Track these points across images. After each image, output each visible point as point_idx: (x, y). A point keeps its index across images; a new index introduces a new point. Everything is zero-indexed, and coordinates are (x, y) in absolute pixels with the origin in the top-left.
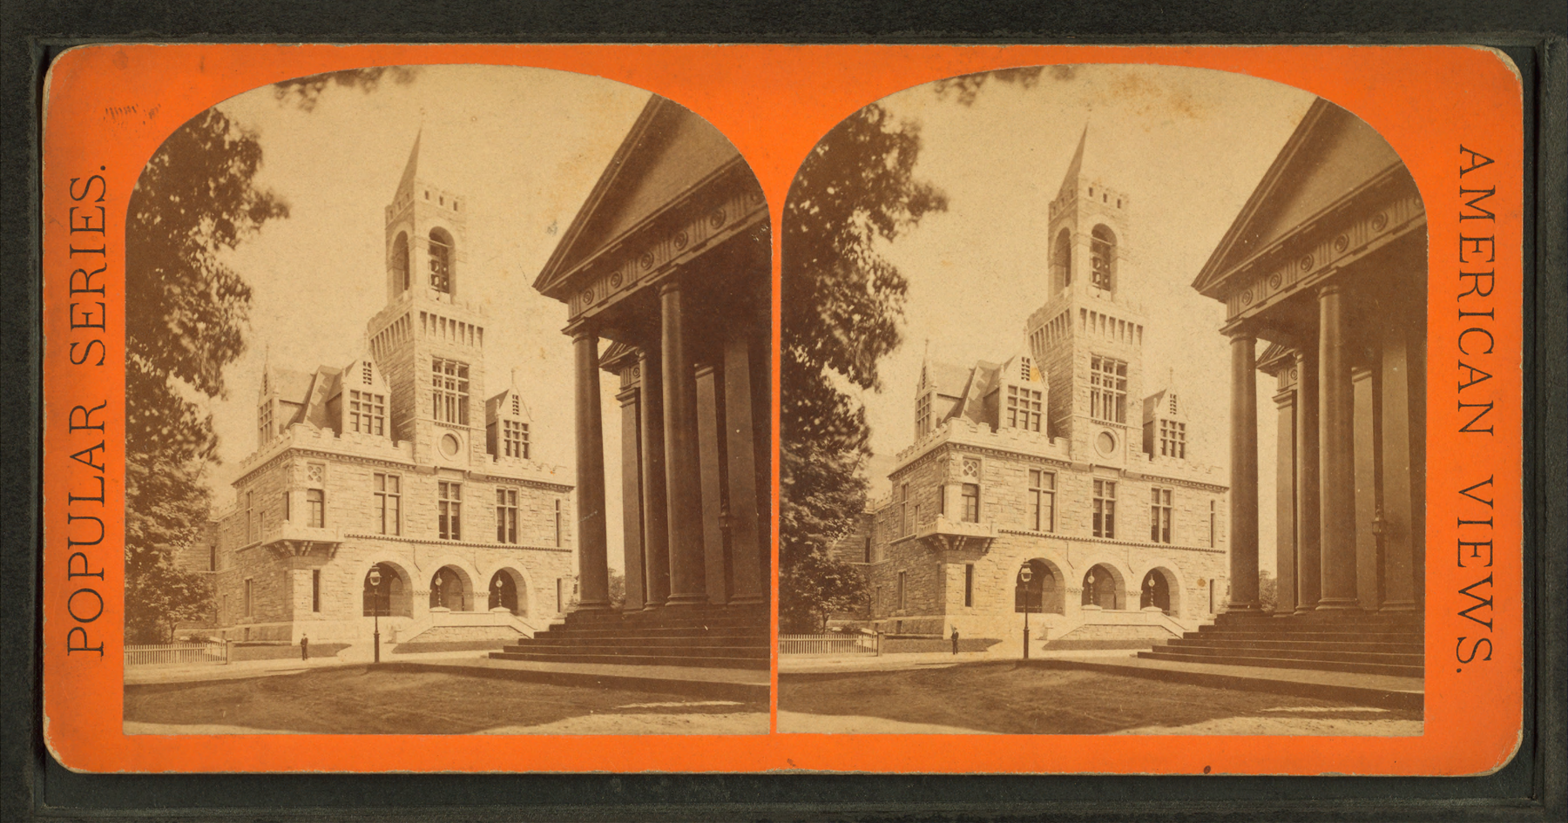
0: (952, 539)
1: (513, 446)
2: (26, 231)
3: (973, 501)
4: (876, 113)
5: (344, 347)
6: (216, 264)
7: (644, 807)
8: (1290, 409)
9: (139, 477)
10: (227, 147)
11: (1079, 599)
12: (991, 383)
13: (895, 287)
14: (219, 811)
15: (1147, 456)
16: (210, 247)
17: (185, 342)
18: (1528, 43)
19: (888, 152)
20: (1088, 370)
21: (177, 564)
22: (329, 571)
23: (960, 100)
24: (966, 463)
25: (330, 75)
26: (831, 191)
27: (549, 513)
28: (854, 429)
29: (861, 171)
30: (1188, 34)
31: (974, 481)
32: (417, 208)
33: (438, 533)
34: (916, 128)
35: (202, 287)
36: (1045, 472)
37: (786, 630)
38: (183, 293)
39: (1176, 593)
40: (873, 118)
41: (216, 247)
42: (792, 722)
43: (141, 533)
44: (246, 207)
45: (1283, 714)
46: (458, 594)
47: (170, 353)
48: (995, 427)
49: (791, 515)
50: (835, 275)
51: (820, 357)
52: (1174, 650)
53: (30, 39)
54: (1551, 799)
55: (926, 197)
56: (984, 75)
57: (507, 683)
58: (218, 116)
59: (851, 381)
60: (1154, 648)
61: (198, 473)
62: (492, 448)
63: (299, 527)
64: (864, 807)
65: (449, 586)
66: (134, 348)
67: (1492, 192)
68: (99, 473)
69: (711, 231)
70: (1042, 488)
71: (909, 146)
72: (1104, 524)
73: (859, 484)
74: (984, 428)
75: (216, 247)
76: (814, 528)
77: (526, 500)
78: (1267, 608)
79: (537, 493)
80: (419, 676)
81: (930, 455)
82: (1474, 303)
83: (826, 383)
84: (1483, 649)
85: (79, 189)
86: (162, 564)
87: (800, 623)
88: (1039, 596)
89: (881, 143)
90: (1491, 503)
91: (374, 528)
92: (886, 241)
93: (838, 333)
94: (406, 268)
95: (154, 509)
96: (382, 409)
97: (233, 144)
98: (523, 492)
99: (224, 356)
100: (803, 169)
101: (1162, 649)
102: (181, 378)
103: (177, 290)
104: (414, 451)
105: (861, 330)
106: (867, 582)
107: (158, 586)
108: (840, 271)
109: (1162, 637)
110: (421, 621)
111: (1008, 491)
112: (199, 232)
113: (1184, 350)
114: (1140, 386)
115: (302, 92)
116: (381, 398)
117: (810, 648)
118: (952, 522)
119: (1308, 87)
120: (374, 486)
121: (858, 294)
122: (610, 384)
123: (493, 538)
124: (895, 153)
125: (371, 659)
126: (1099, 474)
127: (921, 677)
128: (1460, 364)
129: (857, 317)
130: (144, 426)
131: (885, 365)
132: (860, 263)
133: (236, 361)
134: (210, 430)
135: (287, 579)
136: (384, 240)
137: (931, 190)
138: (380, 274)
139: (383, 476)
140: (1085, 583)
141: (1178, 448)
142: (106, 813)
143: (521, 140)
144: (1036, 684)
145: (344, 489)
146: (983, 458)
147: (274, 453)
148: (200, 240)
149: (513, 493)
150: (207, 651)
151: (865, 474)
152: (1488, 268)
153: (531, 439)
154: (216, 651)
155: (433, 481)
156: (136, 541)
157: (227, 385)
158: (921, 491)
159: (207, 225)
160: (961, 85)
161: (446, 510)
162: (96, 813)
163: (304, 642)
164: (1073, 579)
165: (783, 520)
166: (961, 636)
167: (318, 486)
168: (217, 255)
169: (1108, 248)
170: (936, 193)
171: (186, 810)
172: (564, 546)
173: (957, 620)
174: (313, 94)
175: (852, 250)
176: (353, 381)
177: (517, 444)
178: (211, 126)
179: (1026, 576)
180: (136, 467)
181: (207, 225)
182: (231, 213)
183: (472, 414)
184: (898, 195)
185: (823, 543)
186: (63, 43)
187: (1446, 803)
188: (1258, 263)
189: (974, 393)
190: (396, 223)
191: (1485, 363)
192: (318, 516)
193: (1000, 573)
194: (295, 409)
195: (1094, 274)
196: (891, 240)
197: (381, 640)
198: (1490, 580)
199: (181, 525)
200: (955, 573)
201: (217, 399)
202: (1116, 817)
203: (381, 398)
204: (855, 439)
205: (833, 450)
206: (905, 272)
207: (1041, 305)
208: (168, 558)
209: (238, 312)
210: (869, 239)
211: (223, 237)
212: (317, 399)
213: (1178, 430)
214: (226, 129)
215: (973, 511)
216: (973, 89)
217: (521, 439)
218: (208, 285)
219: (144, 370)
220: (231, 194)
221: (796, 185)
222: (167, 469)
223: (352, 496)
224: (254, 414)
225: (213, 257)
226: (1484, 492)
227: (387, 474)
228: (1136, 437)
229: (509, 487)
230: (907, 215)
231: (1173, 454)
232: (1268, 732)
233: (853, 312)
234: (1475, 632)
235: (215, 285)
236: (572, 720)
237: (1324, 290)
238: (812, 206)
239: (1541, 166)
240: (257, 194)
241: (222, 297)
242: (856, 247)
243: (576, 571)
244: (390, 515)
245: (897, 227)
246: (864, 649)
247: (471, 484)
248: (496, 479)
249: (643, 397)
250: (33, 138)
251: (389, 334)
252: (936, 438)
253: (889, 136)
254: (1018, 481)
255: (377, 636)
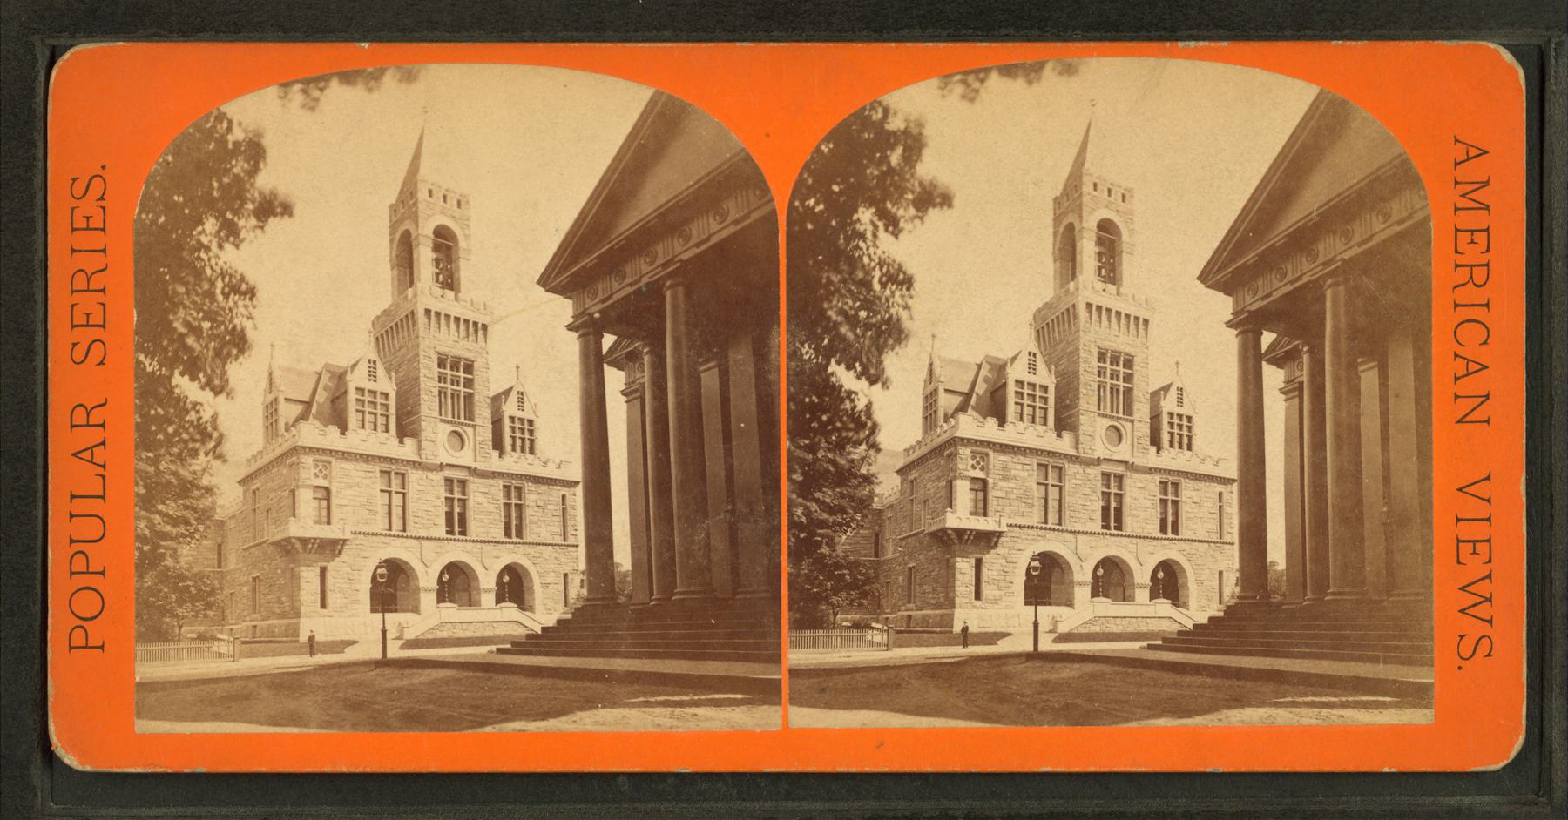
0: (960, 533)
1: (519, 442)
2: (33, 231)
3: (324, 503)
4: (880, 110)
5: (1010, 338)
6: (221, 263)
7: (649, 806)
8: (1296, 401)
9: (145, 476)
10: (230, 146)
11: (434, 596)
12: (338, 387)
13: (901, 283)
14: (225, 810)
15: (1154, 449)
16: (214, 247)
17: (190, 341)
18: (1535, 41)
19: (892, 149)
20: (1095, 363)
21: (183, 562)
22: (993, 561)
23: (964, 97)
24: (316, 466)
25: (332, 75)
26: (836, 188)
27: (554, 509)
28: (863, 425)
29: (868, 168)
30: (1195, 32)
31: (981, 475)
32: (1085, 199)
33: (1100, 523)
34: (920, 125)
35: (206, 286)
36: (1051, 465)
37: (797, 625)
38: (187, 293)
39: (1185, 585)
40: (877, 115)
41: (220, 247)
42: (805, 717)
43: (147, 532)
44: (250, 206)
45: (1294, 704)
46: (465, 590)
47: (176, 352)
48: (343, 429)
49: (799, 512)
50: (839, 272)
51: (828, 353)
52: (1182, 641)
53: (36, 39)
54: (1558, 795)
55: (270, 203)
56: (987, 71)
57: (515, 678)
58: (221, 117)
59: (859, 378)
60: (1165, 640)
61: (204, 470)
62: (498, 444)
63: (305, 525)
64: (872, 805)
65: (456, 584)
66: (140, 348)
67: (1487, 183)
68: (100, 470)
69: (714, 227)
70: (1050, 482)
71: (913, 143)
72: (1113, 517)
73: (209, 490)
74: (334, 431)
75: (220, 247)
76: (823, 524)
77: (532, 496)
78: (1276, 599)
79: (543, 488)
80: (427, 671)
81: (938, 451)
82: (1469, 294)
83: (833, 379)
84: (1484, 647)
85: (79, 188)
86: (169, 562)
87: (810, 619)
88: (1049, 588)
89: (887, 140)
90: (1488, 501)
91: (380, 525)
92: (892, 238)
93: (844, 330)
94: (1073, 260)
95: (818, 495)
96: (1046, 399)
97: (236, 143)
98: (528, 486)
99: (229, 355)
100: (806, 167)
101: (1172, 640)
102: (187, 377)
103: (181, 290)
104: (420, 448)
105: (867, 326)
106: (877, 577)
107: (821, 571)
108: (845, 268)
109: (1171, 628)
110: (431, 616)
111: (1016, 482)
112: (203, 231)
113: (1191, 345)
114: (1148, 379)
115: (305, 92)
116: (386, 396)
117: (819, 644)
118: (960, 517)
119: (1309, 79)
120: (380, 484)
121: (863, 291)
122: (615, 380)
123: (498, 533)
124: (899, 150)
125: (379, 656)
126: (1106, 468)
127: (931, 671)
128: (1456, 355)
129: (863, 314)
130: (803, 413)
131: (893, 362)
132: (866, 260)
133: (241, 359)
134: (215, 429)
135: (295, 577)
136: (1051, 230)
137: (935, 186)
138: (1047, 265)
139: (1046, 466)
140: (440, 581)
141: (1185, 440)
142: (115, 811)
143: (529, 139)
144: (1046, 676)
145: (1005, 478)
146: (333, 460)
147: (279, 451)
148: (205, 240)
149: (519, 489)
150: (215, 648)
151: (873, 469)
152: (1483, 259)
153: (1195, 430)
154: (224, 648)
155: (438, 477)
156: (142, 539)
157: (231, 384)
158: (929, 485)
159: (210, 225)
160: (964, 82)
161: (452, 507)
162: (103, 812)
163: (311, 639)
164: (428, 578)
165: (791, 514)
166: (971, 630)
167: (324, 483)
168: (221, 254)
169: (449, 248)
170: (281, 198)
171: (193, 809)
172: (571, 540)
173: (967, 615)
174: (316, 93)
175: (858, 247)
176: (1017, 372)
177: (1181, 436)
178: (214, 127)
179: (1035, 569)
180: (142, 466)
181: (210, 225)
182: (236, 213)
183: (477, 411)
184: (244, 201)
185: (832, 539)
186: (70, 42)
187: (1454, 801)
188: (1262, 256)
189: (981, 388)
190: (401, 221)
191: (1483, 355)
192: (324, 513)
193: (1009, 566)
194: (300, 407)
195: (1100, 268)
196: (896, 236)
197: (1040, 629)
198: (1489, 576)
199: (187, 523)
200: (964, 567)
201: (222, 397)
202: (1123, 814)
203: (386, 396)
204: (862, 435)
205: (840, 446)
206: (253, 277)
207: (385, 306)
208: (175, 555)
209: (242, 309)
210: (875, 236)
211: (228, 237)
212: (322, 396)
213: (1185, 422)
214: (229, 129)
215: (981, 505)
216: (976, 85)
217: (527, 436)
218: (213, 284)
219: (149, 369)
220: (236, 194)
221: (800, 183)
222: (173, 467)
223: (358, 492)
224: (260, 414)
225: (217, 257)
226: (1482, 489)
227: (393, 472)
228: (1144, 429)
229: (515, 483)
230: (253, 221)
231: (1181, 447)
232: (1280, 722)
233: (860, 308)
234: (1475, 629)
235: (219, 284)
236: (580, 714)
237: (1329, 282)
238: (817, 203)
239: (1546, 164)
240: (921, 183)
241: (226, 296)
242: (862, 244)
243: (582, 566)
244: (397, 511)
245: (902, 224)
246: (873, 644)
247: (477, 480)
248: (501, 475)
249: (648, 397)
250: (38, 137)
251: (394, 331)
252: (943, 432)
253: (894, 133)
254: (1025, 473)
255: (384, 632)
